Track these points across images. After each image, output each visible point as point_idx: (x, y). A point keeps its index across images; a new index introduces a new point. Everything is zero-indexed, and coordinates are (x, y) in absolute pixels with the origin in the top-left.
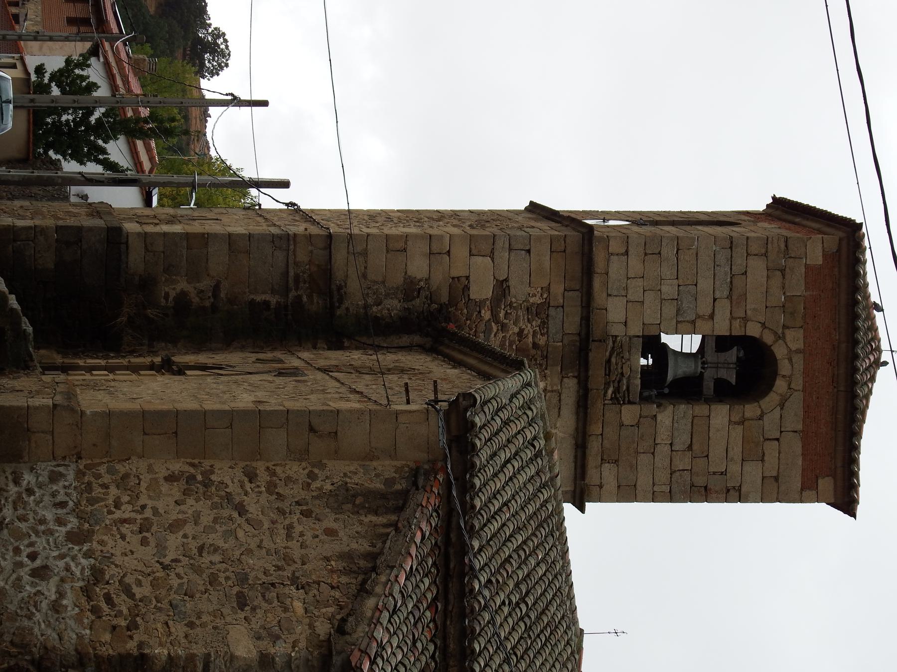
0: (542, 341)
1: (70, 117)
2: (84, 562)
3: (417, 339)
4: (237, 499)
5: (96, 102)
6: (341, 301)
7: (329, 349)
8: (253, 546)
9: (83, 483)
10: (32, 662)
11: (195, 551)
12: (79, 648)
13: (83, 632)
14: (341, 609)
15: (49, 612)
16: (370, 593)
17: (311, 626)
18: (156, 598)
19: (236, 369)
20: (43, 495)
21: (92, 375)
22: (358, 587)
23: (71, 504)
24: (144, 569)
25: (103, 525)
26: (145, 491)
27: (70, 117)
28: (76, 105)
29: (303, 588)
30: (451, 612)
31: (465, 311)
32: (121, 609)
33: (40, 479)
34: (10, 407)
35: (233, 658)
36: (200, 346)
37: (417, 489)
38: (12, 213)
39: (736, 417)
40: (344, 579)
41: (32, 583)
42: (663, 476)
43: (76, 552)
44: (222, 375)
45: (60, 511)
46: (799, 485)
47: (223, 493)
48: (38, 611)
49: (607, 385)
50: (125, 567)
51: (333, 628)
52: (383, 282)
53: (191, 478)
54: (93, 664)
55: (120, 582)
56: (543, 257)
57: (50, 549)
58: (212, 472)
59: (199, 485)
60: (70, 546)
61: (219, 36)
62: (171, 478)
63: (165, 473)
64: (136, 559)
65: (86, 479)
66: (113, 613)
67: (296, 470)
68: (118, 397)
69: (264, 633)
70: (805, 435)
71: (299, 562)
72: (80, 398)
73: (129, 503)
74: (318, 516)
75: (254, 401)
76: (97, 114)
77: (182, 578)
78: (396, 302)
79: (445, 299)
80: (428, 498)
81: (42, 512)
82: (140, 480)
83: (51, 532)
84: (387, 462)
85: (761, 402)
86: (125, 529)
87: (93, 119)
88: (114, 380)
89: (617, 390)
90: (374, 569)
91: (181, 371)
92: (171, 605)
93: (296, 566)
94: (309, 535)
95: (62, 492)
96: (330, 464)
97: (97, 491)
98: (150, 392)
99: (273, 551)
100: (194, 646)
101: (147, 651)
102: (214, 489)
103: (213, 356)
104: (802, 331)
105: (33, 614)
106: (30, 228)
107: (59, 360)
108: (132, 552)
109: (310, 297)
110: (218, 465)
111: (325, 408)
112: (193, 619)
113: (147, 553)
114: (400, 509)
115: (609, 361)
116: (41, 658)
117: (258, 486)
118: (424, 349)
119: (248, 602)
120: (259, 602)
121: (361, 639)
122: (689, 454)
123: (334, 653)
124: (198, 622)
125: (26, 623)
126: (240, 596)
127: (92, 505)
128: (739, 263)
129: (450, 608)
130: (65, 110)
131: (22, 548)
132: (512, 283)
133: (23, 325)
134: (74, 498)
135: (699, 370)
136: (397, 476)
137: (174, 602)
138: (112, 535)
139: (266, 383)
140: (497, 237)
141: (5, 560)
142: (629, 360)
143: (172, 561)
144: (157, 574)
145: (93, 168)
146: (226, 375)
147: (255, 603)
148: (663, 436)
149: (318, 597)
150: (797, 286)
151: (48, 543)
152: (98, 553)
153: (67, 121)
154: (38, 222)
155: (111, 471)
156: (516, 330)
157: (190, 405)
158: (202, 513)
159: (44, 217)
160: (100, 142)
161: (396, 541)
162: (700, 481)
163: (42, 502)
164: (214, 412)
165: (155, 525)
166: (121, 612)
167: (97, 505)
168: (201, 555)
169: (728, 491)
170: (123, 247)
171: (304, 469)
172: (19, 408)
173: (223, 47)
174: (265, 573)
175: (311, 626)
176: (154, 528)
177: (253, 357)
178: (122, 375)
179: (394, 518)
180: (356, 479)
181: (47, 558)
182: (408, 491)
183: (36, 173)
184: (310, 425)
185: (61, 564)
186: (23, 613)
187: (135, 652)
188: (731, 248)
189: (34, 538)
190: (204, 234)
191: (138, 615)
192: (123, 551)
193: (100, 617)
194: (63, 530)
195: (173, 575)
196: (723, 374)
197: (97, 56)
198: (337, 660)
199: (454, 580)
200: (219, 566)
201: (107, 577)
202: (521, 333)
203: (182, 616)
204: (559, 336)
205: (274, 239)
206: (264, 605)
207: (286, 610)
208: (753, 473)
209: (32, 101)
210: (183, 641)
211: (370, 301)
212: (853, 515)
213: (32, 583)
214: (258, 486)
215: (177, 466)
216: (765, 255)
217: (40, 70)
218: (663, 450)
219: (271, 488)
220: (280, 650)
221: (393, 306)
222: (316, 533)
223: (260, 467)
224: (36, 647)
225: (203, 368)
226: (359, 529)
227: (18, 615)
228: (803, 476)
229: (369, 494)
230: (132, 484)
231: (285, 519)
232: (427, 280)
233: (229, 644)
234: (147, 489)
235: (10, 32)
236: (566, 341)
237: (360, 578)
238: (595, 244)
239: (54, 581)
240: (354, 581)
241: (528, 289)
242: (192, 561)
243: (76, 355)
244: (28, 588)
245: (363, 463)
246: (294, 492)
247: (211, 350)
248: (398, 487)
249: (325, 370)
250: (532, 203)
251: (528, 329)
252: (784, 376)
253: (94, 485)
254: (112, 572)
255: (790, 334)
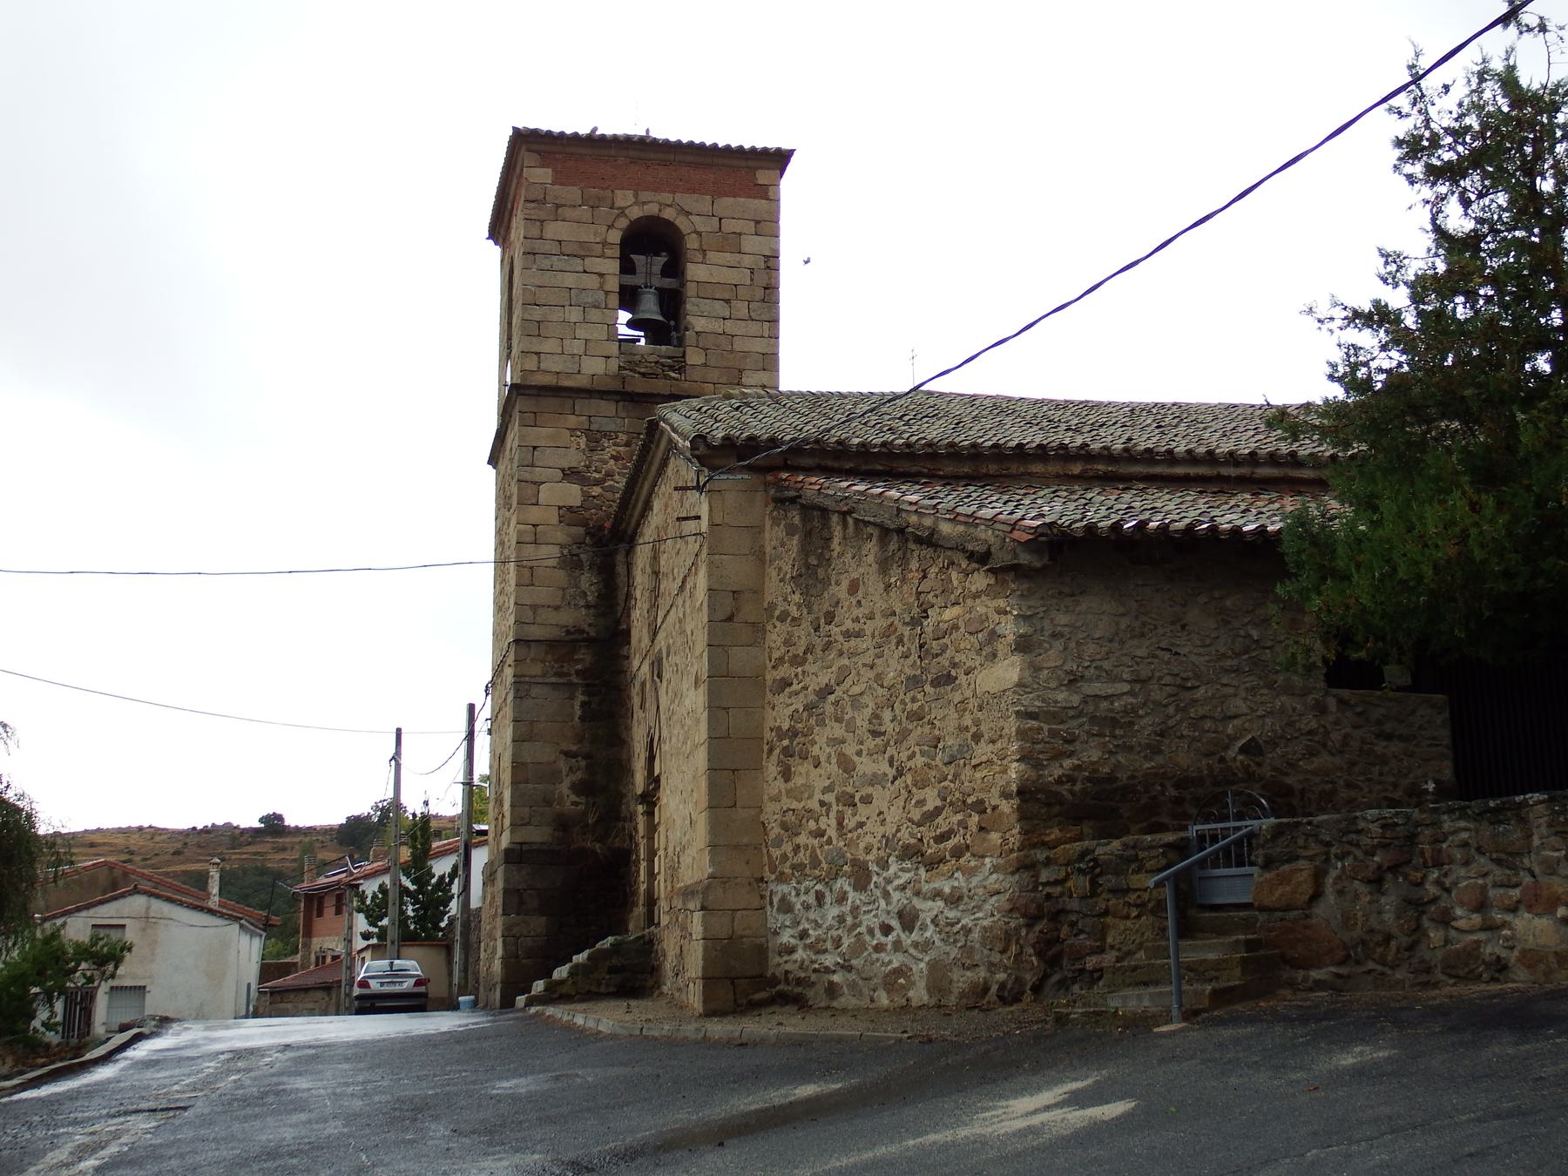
0: (623, 438)
1: (410, 908)
2: (893, 869)
3: (620, 558)
4: (812, 697)
5: (395, 884)
6: (582, 631)
7: (629, 643)
8: (871, 674)
9: (793, 874)
10: (1029, 926)
11: (878, 740)
12: (1011, 869)
13: (988, 866)
14: (953, 563)
15: (960, 908)
16: (933, 531)
17: (976, 596)
18: (940, 782)
19: (652, 724)
20: (808, 919)
21: (659, 873)
22: (924, 547)
23: (819, 887)
24: (902, 798)
25: (845, 848)
26: (803, 804)
27: (410, 908)
28: (397, 902)
29: (925, 611)
30: (929, 469)
31: (593, 511)
32: (956, 822)
33: (788, 923)
34: (705, 959)
35: (1020, 684)
36: (625, 770)
37: (800, 497)
38: (491, 959)
39: (699, 257)
40: (914, 565)
41: (921, 929)
42: (753, 328)
43: (881, 879)
44: (660, 737)
45: (828, 899)
46: (764, 201)
47: (805, 714)
48: (959, 921)
49: (666, 377)
50: (900, 821)
51: (978, 570)
52: (564, 589)
53: (787, 752)
54: (1032, 852)
55: (919, 825)
56: (541, 434)
57: (877, 909)
58: (779, 728)
59: (795, 743)
60: (872, 886)
61: (377, 806)
62: (787, 775)
63: (780, 781)
64: (889, 808)
65: (788, 871)
66: (962, 831)
67: (776, 635)
68: (689, 840)
69: (987, 650)
70: (717, 193)
71: (891, 619)
72: (689, 883)
73: (817, 821)
74: (833, 604)
75: (695, 687)
76: (407, 883)
77: (914, 754)
78: (583, 578)
79: (581, 530)
80: (811, 484)
81: (829, 921)
82: (789, 810)
83: (855, 910)
84: (767, 535)
85: (685, 233)
86: (850, 823)
87: (412, 888)
88: (666, 849)
89: (671, 368)
90: (901, 531)
91: (654, 781)
92: (950, 763)
93: (896, 622)
94: (857, 612)
95: (803, 898)
96: (769, 598)
97: (803, 857)
98: (681, 807)
99: (878, 650)
100: (1006, 731)
101: (1014, 788)
102: (800, 725)
103: (636, 755)
104: (616, 191)
105: (963, 927)
106: (504, 942)
107: (640, 910)
108: (881, 813)
109: (577, 661)
110: (770, 723)
111: (705, 605)
112: (969, 735)
113: (881, 796)
114: (824, 511)
115: (643, 375)
116: (1024, 916)
117: (796, 675)
118: (630, 551)
119: (945, 672)
120: (944, 661)
121: (997, 532)
122: (733, 302)
123: (1016, 562)
124: (974, 729)
125: (975, 935)
126: (936, 683)
127: (820, 862)
128: (548, 247)
129: (926, 471)
130: (402, 912)
131: (875, 942)
132: (566, 465)
133: (605, 946)
134: (812, 884)
135: (652, 290)
136: (783, 522)
137: (946, 760)
138: (858, 837)
139: (670, 687)
140: (521, 478)
141: (890, 962)
142: (642, 356)
143: (891, 765)
144: (909, 782)
145: (455, 889)
146: (660, 733)
147: (947, 664)
148: (717, 326)
149: (938, 592)
150: (571, 193)
151: (869, 912)
152: (882, 853)
153: (413, 910)
154: (499, 934)
155: (778, 842)
156: (612, 462)
157: (701, 759)
158: (830, 736)
159: (495, 928)
160: (434, 881)
161: (865, 511)
162: (759, 293)
163: (816, 921)
164: (711, 728)
165: (845, 788)
166: (960, 823)
167: (820, 857)
168: (884, 734)
169: (768, 267)
170: (524, 847)
171: (775, 627)
172: (706, 949)
173: (385, 803)
174: (907, 657)
175: (976, 596)
176: (849, 789)
177: (638, 713)
178: (660, 840)
179: (835, 518)
180: (787, 568)
181: (888, 913)
182: (803, 506)
183: (458, 937)
184: (725, 621)
185: (896, 896)
186: (963, 939)
187: (1015, 802)
188: (534, 254)
189: (862, 929)
190: (513, 767)
191: (964, 802)
192: (879, 823)
193: (968, 847)
194: (852, 895)
195: (910, 764)
196: (657, 269)
197: (358, 885)
198: (1025, 558)
199: (895, 465)
200: (898, 712)
201: (913, 841)
202: (616, 458)
203: (966, 749)
204: (619, 421)
205: (518, 697)
206: (948, 654)
207: (956, 627)
208: (750, 243)
209: (393, 943)
210: (999, 745)
211: (582, 603)
212: (791, 152)
213: (921, 929)
214: (796, 675)
215: (772, 768)
216: (542, 222)
217: (366, 936)
218: (729, 326)
219: (798, 661)
220: (1009, 629)
221: (588, 581)
222: (854, 603)
223: (771, 676)
224: (1009, 923)
225: (651, 759)
226: (850, 555)
227: (965, 945)
228: (755, 198)
229: (805, 551)
230: (793, 818)
231: (836, 641)
232: (562, 546)
233: (1002, 689)
234: (800, 801)
235: (344, 962)
236: (624, 415)
237: (912, 546)
238: (528, 383)
239: (918, 903)
240: (916, 554)
241: (572, 450)
242: (892, 743)
243: (635, 893)
244: (928, 934)
245: (768, 562)
246: (803, 635)
247: (629, 760)
248: (797, 520)
249: (654, 634)
250: (489, 463)
251: (612, 450)
252: (660, 210)
253: (795, 861)
254: (907, 836)
255: (620, 203)
